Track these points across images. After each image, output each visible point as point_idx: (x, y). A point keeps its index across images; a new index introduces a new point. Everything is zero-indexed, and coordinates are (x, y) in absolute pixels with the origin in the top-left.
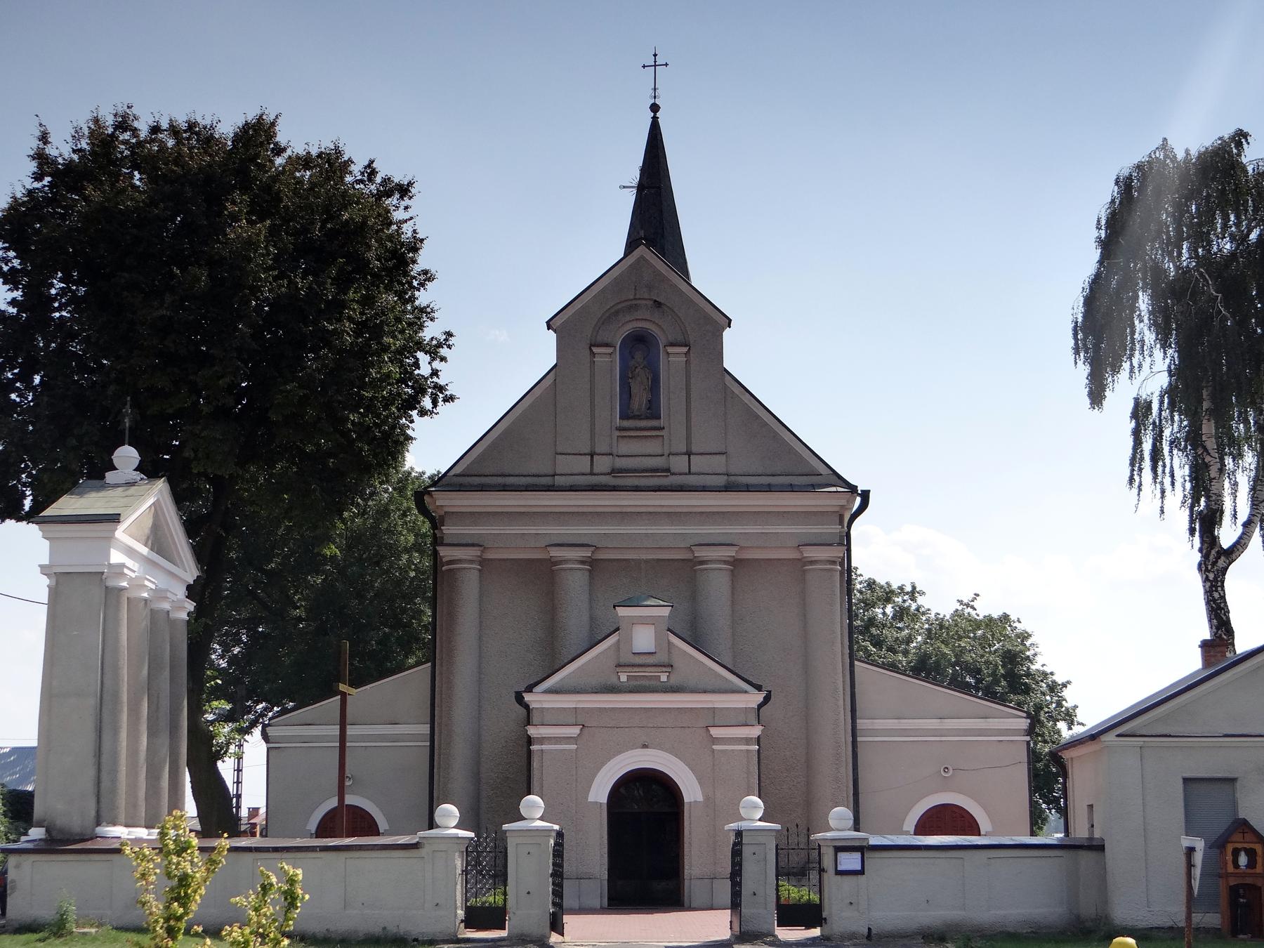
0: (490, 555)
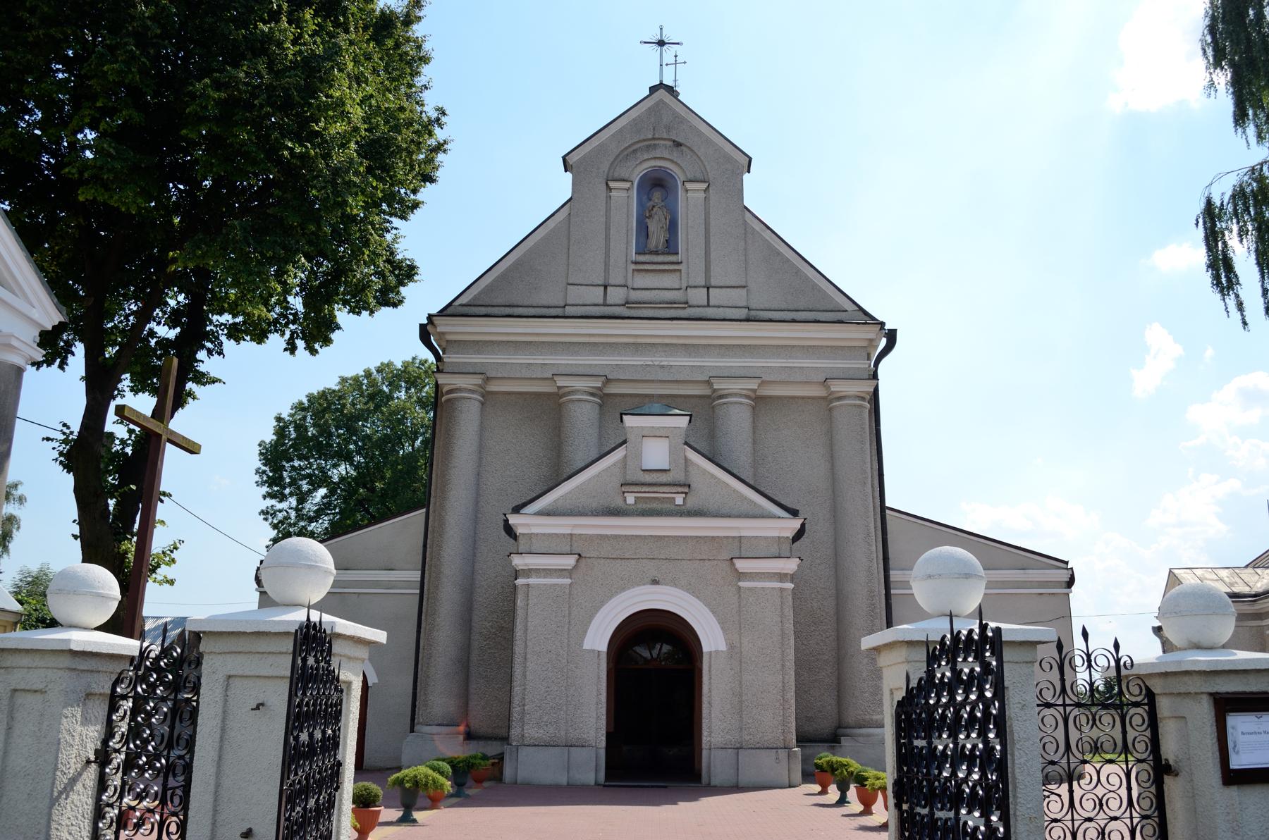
0: (493, 387)
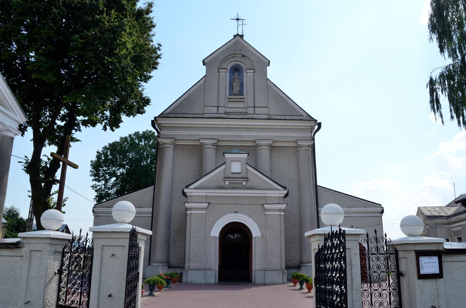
0: (178, 143)
